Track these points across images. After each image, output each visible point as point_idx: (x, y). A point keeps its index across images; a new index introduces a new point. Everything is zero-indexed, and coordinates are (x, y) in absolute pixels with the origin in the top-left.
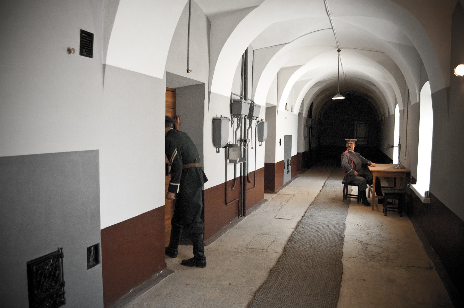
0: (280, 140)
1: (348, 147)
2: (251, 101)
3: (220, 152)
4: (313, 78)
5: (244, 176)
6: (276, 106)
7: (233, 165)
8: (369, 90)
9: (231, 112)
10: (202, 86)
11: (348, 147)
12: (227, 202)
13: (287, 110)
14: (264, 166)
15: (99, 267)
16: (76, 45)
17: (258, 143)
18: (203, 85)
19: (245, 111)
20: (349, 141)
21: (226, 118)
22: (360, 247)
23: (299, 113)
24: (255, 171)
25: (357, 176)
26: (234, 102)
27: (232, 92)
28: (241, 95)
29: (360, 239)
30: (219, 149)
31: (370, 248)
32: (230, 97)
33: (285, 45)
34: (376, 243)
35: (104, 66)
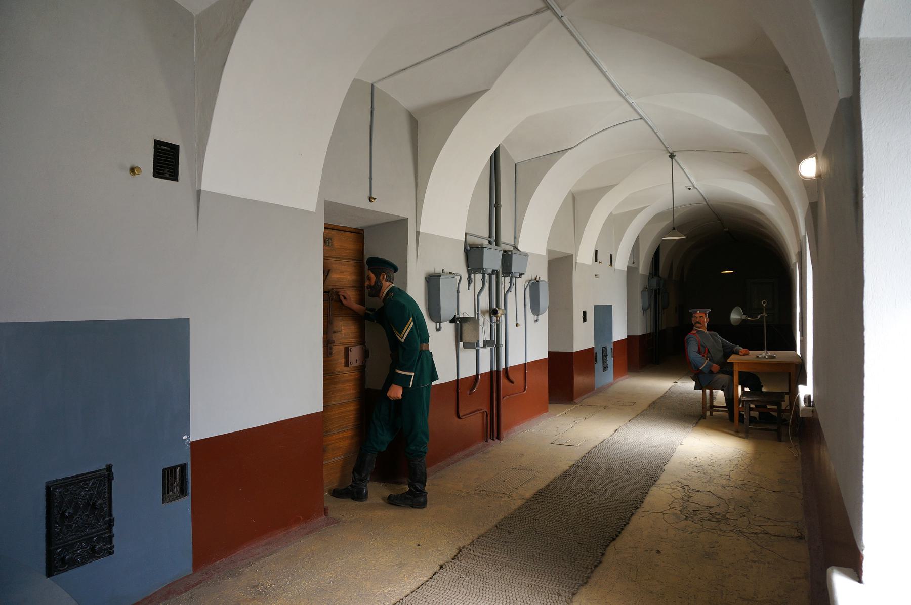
0: (585, 313)
1: (695, 323)
2: (513, 247)
3: (442, 329)
4: (644, 208)
5: (498, 371)
6: (572, 255)
7: (473, 352)
8: (759, 224)
9: (468, 264)
10: (402, 223)
11: (695, 323)
12: (461, 414)
13: (600, 262)
14: (547, 357)
15: (185, 505)
16: (147, 162)
17: (531, 316)
18: (405, 221)
19: (492, 260)
20: (696, 312)
21: (454, 273)
22: (679, 494)
23: (629, 268)
24: (525, 363)
25: (718, 373)
26: (471, 248)
27: (467, 232)
28: (489, 237)
29: (685, 482)
30: (440, 325)
31: (696, 497)
32: (464, 240)
33: (567, 152)
34: (712, 489)
35: (199, 192)
